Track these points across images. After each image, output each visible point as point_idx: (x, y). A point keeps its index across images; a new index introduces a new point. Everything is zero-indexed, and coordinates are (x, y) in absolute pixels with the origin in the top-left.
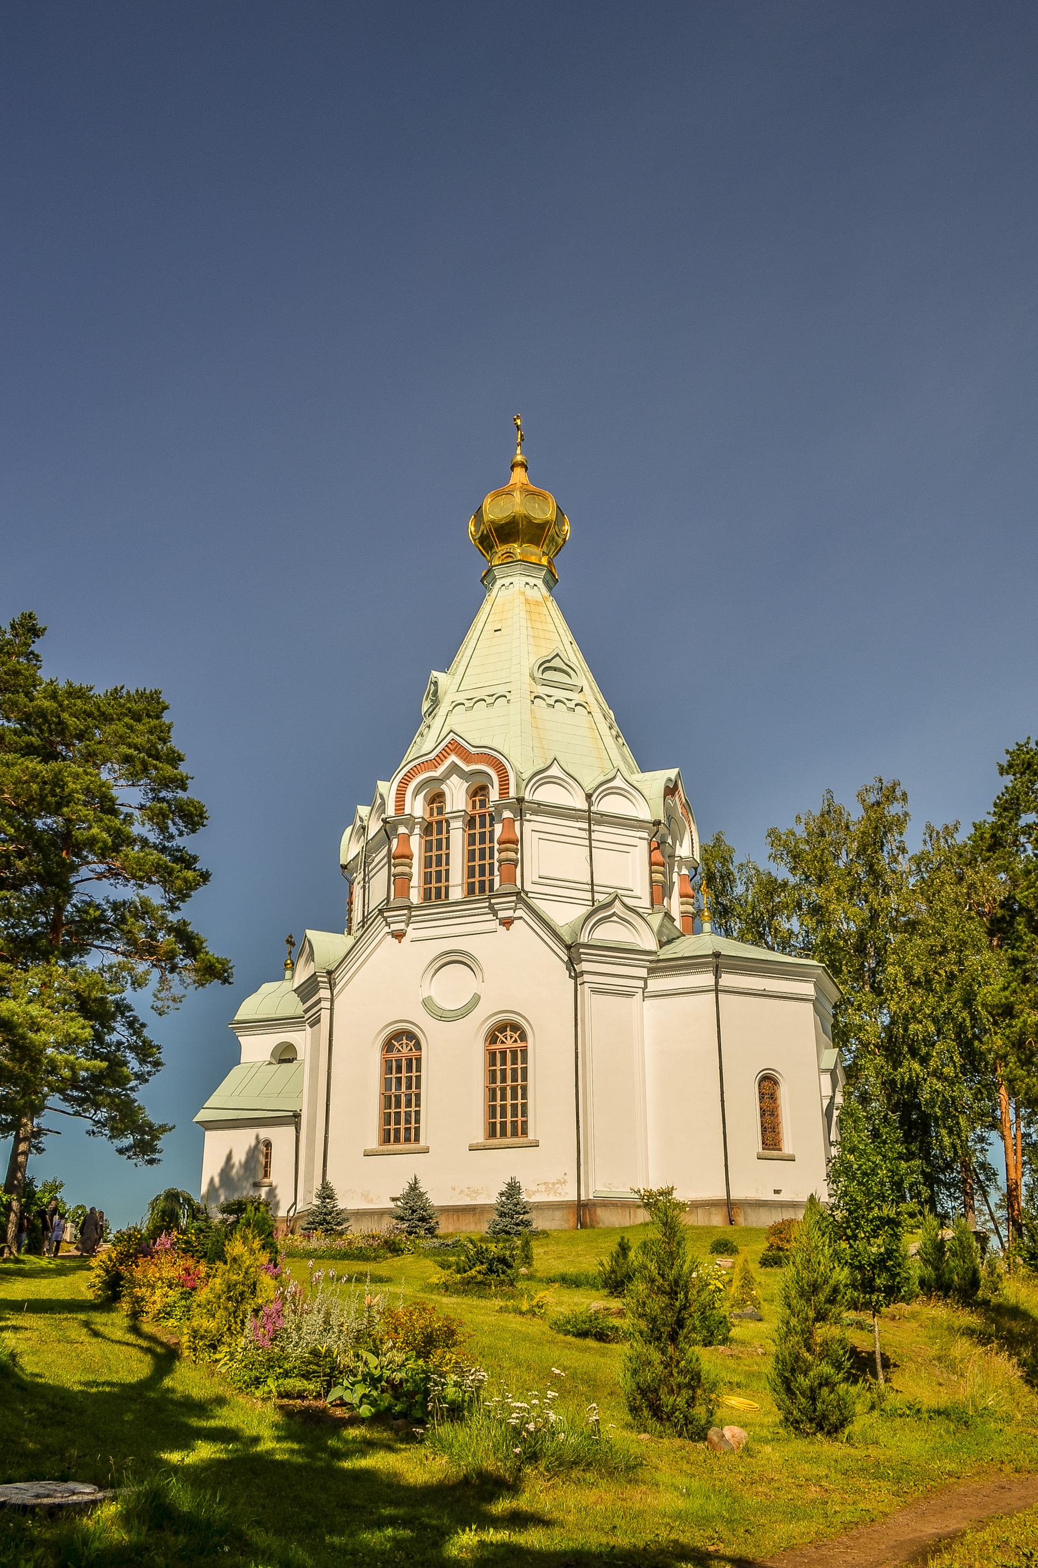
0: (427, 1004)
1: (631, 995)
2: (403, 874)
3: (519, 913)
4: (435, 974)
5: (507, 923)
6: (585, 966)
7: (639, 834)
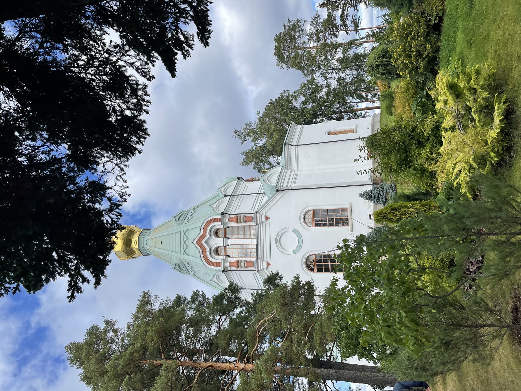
0: (295, 252)
2: (244, 263)
3: (264, 213)
4: (283, 248)
5: (267, 218)
6: (285, 185)
7: (235, 199)
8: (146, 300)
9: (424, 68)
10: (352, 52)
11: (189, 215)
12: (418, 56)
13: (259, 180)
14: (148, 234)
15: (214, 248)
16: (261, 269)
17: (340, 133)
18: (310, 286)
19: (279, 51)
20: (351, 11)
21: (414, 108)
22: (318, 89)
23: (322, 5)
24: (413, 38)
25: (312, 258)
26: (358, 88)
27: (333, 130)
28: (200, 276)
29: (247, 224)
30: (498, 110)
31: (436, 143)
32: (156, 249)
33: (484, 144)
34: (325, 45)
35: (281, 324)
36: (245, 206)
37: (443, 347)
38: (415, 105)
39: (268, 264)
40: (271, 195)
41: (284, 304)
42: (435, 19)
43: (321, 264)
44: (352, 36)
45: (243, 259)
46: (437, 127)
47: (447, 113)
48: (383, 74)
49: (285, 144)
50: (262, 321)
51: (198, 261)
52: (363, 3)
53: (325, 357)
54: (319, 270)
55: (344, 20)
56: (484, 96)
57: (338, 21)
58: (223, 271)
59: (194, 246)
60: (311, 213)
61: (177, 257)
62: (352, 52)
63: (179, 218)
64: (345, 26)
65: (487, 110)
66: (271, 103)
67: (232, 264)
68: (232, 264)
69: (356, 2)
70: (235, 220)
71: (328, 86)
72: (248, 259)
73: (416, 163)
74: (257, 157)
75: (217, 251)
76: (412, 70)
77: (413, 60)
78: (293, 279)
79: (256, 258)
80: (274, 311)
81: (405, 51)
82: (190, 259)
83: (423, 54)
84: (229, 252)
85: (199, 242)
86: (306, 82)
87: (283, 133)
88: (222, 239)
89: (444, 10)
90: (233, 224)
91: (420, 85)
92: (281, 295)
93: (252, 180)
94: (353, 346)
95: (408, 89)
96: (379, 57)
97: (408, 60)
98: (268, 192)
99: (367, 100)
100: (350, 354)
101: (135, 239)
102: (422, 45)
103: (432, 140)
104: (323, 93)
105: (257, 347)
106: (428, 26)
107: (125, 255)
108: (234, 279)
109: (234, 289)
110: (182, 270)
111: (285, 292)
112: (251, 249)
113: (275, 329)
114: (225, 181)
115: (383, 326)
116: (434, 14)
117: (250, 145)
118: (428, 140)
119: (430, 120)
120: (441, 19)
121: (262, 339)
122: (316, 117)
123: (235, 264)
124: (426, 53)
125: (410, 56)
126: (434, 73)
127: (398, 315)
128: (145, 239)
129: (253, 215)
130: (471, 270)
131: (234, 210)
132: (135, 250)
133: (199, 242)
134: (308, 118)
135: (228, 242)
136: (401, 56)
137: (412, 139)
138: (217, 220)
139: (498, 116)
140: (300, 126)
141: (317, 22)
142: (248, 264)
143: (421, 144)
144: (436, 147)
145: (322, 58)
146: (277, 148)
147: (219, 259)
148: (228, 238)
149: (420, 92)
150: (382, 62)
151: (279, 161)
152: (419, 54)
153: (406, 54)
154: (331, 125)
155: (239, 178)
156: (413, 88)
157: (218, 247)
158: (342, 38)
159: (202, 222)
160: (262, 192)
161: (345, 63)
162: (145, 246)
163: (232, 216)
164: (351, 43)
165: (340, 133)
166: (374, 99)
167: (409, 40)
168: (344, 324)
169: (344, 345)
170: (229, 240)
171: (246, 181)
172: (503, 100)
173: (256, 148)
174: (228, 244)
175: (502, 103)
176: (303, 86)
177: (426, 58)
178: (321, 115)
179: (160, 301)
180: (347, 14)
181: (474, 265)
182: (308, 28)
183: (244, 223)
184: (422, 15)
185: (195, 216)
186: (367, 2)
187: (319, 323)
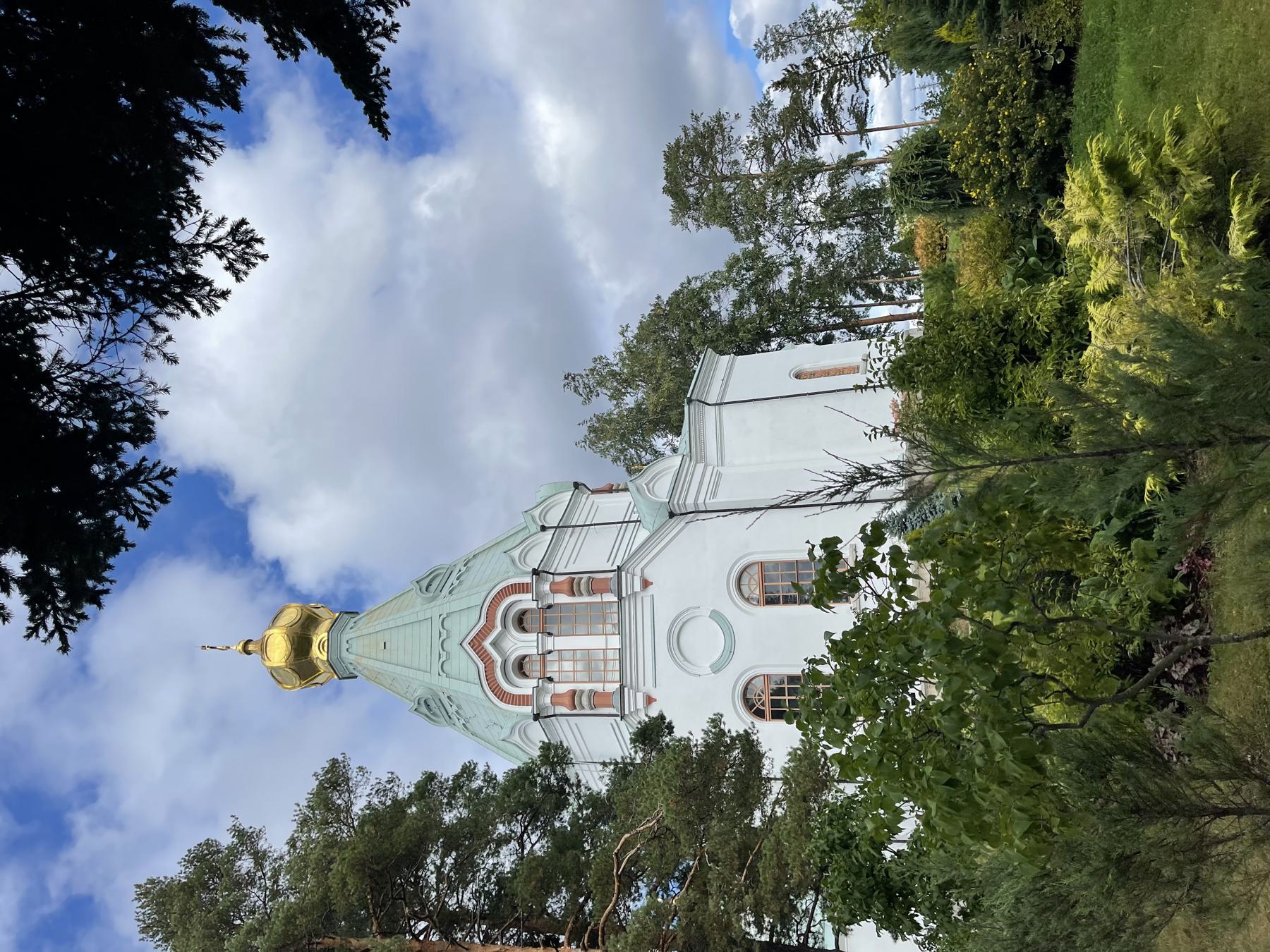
0: (717, 668)
1: (719, 475)
2: (589, 697)
4: (686, 660)
5: (646, 584)
6: (690, 501)
7: (567, 537)
8: (335, 778)
9: (1031, 177)
10: (852, 181)
11: (453, 578)
12: (1014, 147)
13: (626, 490)
14: (351, 624)
15: (513, 658)
16: (631, 713)
17: (826, 373)
18: (748, 743)
19: (676, 185)
20: (848, 90)
21: (1007, 283)
22: (770, 270)
23: (777, 85)
24: (1001, 103)
25: (759, 683)
26: (867, 273)
27: (808, 367)
28: (478, 731)
29: (596, 599)
30: (1239, 214)
31: (1069, 349)
32: (371, 662)
33: (1203, 316)
34: (786, 167)
35: (678, 842)
36: (591, 554)
37: (1113, 870)
38: (1010, 276)
39: (649, 700)
40: (656, 526)
41: (687, 792)
42: (1057, 55)
43: (780, 699)
44: (852, 145)
45: (587, 687)
46: (1072, 309)
47: (1099, 254)
48: (929, 197)
49: (690, 401)
50: (627, 835)
51: (475, 690)
52: (878, 74)
53: (795, 937)
54: (777, 716)
55: (830, 110)
56: (1199, 187)
57: (817, 110)
58: (536, 717)
59: (463, 652)
60: (756, 569)
61: (425, 681)
62: (852, 181)
63: (429, 585)
64: (835, 123)
65: (1210, 224)
66: (658, 306)
67: (558, 700)
68: (558, 700)
69: (860, 73)
70: (566, 587)
71: (796, 262)
72: (598, 687)
73: (1018, 401)
74: (623, 435)
75: (521, 666)
76: (1001, 183)
77: (1003, 156)
78: (706, 726)
79: (618, 685)
80: (659, 810)
81: (981, 134)
82: (455, 686)
83: (1028, 141)
84: (552, 670)
85: (476, 644)
86: (739, 253)
87: (685, 376)
88: (534, 636)
89: (1079, 28)
90: (562, 599)
91: (1021, 224)
92: (677, 767)
93: (610, 490)
94: (862, 893)
95: (992, 237)
96: (918, 156)
97: (989, 156)
98: (648, 520)
99: (890, 300)
100: (855, 916)
101: (320, 636)
102: (1024, 119)
103: (1059, 343)
104: (783, 282)
105: (616, 904)
106: (1039, 72)
107: (294, 678)
108: (563, 739)
109: (555, 755)
110: (434, 714)
111: (688, 761)
112: (605, 661)
113: (662, 856)
114: (544, 492)
115: (936, 782)
116: (1054, 42)
117: (604, 404)
118: (1047, 342)
119: (1052, 289)
120: (1071, 52)
121: (628, 882)
122: (767, 338)
123: (567, 700)
124: (1035, 137)
125: (995, 147)
126: (1057, 189)
127: (980, 747)
128: (345, 637)
129: (611, 575)
130: (1176, 677)
131: (563, 563)
132: (319, 664)
133: (476, 644)
134: (747, 339)
135: (551, 643)
136: (971, 150)
137: (1004, 340)
138: (523, 588)
139: (1242, 230)
140: (725, 359)
141: (767, 116)
142: (597, 699)
143: (1028, 355)
144: (1070, 358)
145: (781, 197)
146: (668, 416)
147: (526, 687)
148: (550, 634)
149: (1023, 241)
150: (925, 166)
151: (677, 444)
152: (1018, 141)
153: (984, 142)
154: (806, 354)
155: (576, 485)
156: (1004, 235)
157: (525, 656)
158: (828, 149)
159: (484, 594)
160: (634, 518)
161: (835, 212)
162: (344, 654)
163: (558, 579)
164: (850, 163)
165: (826, 373)
166: (911, 297)
167: (991, 107)
168: (837, 835)
169: (836, 889)
170: (550, 639)
171: (594, 492)
172: (1251, 193)
173: (619, 414)
174: (550, 648)
175: (1250, 200)
176: (733, 263)
177: (1034, 150)
178: (777, 335)
179: (373, 782)
180: (839, 96)
181: (1184, 664)
182: (745, 132)
183: (589, 595)
184: (1022, 45)
185: (469, 579)
186: (888, 72)
187: (773, 839)
